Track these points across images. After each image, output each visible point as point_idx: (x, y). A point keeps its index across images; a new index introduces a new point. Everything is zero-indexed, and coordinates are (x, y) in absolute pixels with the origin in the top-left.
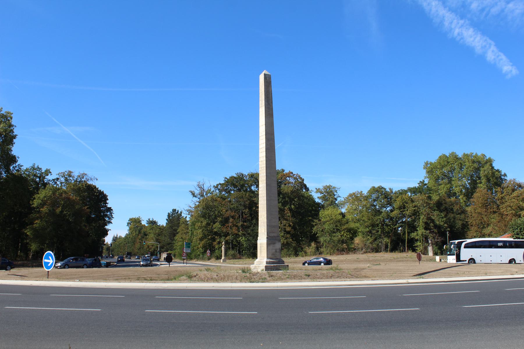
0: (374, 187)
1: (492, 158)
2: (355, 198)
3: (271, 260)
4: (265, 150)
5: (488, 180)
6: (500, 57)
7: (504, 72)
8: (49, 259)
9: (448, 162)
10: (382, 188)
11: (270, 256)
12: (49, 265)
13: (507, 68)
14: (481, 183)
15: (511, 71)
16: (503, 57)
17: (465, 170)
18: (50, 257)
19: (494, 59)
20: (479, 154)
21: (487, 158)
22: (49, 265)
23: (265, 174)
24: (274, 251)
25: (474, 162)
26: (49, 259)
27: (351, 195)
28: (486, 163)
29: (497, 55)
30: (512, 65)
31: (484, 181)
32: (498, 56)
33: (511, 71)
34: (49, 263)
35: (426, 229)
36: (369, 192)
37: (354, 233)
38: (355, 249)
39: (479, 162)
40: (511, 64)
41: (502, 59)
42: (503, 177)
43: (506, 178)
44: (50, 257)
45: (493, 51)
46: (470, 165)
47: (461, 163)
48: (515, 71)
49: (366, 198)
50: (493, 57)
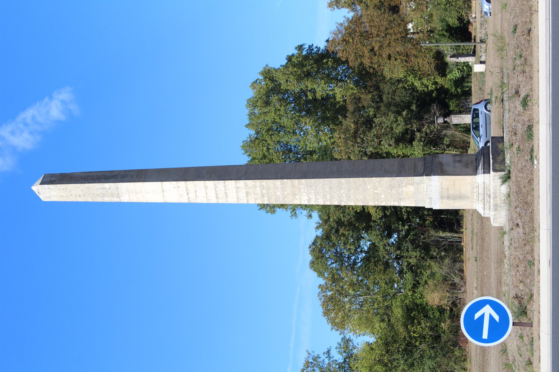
0: (312, 263)
1: (261, 69)
2: (334, 306)
3: (480, 167)
4: (221, 182)
5: (308, 75)
6: (29, 120)
7: (63, 117)
8: (483, 316)
9: (264, 157)
10: (313, 244)
11: (470, 170)
12: (497, 318)
13: (54, 109)
14: (313, 91)
15: (63, 102)
16: (28, 114)
17: (286, 121)
18: (477, 316)
19: (31, 133)
20: (251, 93)
21: (261, 77)
22: (497, 318)
23: (278, 182)
24: (458, 165)
25: (267, 103)
26: (483, 316)
27: (326, 313)
28: (272, 80)
29: (21, 126)
30: (51, 98)
31: (309, 84)
32: (26, 124)
33: (63, 102)
34: (491, 316)
35: (411, 141)
36: (321, 274)
37: (415, 311)
38: (454, 304)
39: (270, 92)
40: (47, 99)
41: (33, 118)
42: (304, 53)
43: (306, 47)
44: (477, 316)
45: (13, 133)
46: (273, 109)
47: (268, 130)
48: (65, 95)
49: (335, 279)
50: (26, 135)
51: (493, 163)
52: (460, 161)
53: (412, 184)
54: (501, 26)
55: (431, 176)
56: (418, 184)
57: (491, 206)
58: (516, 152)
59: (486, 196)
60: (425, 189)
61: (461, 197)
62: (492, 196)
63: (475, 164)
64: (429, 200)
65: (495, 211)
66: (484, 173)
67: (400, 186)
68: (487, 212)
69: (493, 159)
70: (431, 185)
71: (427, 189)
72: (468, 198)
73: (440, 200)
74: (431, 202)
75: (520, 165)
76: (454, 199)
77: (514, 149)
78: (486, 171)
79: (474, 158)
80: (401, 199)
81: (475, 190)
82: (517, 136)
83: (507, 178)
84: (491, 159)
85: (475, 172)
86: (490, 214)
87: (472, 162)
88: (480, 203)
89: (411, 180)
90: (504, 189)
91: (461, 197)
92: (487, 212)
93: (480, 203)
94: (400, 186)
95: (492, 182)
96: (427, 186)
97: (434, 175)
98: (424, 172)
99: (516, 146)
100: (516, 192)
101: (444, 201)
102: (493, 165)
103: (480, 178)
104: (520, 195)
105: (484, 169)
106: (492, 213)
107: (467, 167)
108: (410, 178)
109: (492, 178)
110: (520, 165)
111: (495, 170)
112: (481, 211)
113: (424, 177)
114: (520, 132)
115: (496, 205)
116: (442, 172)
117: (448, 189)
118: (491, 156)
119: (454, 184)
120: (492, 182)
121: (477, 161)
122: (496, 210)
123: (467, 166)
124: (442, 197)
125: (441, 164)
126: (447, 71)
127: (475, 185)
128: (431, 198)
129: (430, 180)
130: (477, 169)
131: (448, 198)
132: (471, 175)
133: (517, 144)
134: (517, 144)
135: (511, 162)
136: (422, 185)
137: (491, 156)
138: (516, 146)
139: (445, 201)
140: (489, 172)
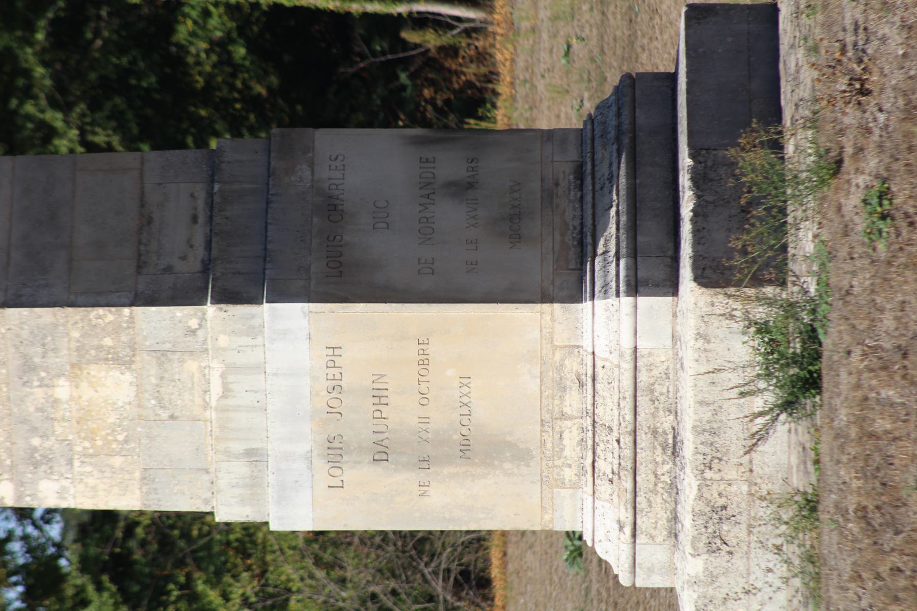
3: (610, 238)
24: (450, 214)
51: (697, 213)
52: (463, 189)
53: (120, 360)
54: (675, 437)
55: (254, 300)
56: (162, 356)
57: (687, 520)
58: (861, 224)
59: (645, 445)
60: (216, 388)
61: (470, 449)
62: (688, 450)
63: (570, 213)
64: (240, 469)
65: (712, 550)
66: (635, 288)
67: (28, 368)
68: (653, 554)
69: (698, 181)
70: (260, 368)
71: (227, 392)
72: (521, 456)
73: (322, 467)
74: (254, 487)
75: (888, 322)
76: (424, 462)
77: (853, 201)
78: (651, 275)
79: (563, 164)
80: (38, 461)
81: (574, 402)
82: (871, 103)
83: (800, 377)
84: (685, 180)
85: (571, 287)
86: (672, 570)
87: (549, 196)
88: (604, 488)
89: (117, 330)
90: (783, 453)
91: (470, 449)
92: (653, 554)
93: (604, 488)
94: (28, 368)
95: (688, 355)
96: (230, 369)
97: (283, 294)
98: (207, 267)
99: (860, 180)
100: (862, 513)
101: (350, 475)
102: (697, 232)
103: (607, 323)
104: (889, 539)
105: (634, 254)
106: (693, 566)
107: (516, 237)
108: (105, 316)
109: (689, 326)
110: (888, 322)
111: (707, 276)
112: (611, 548)
113: (210, 310)
114: (896, 78)
115: (717, 513)
116: (341, 277)
117: (379, 396)
118: (685, 161)
119: (424, 363)
120: (688, 355)
121: (587, 182)
122: (716, 544)
123: (512, 225)
124: (335, 451)
125: (331, 208)
126: (47, 602)
127: (572, 365)
128: (254, 456)
129: (254, 331)
130: (583, 248)
131: (381, 453)
132: (546, 298)
133: (872, 163)
134: (872, 163)
135: (824, 285)
136: (192, 365)
137: (685, 161)
138: (860, 180)
139: (359, 474)
140: (671, 286)
